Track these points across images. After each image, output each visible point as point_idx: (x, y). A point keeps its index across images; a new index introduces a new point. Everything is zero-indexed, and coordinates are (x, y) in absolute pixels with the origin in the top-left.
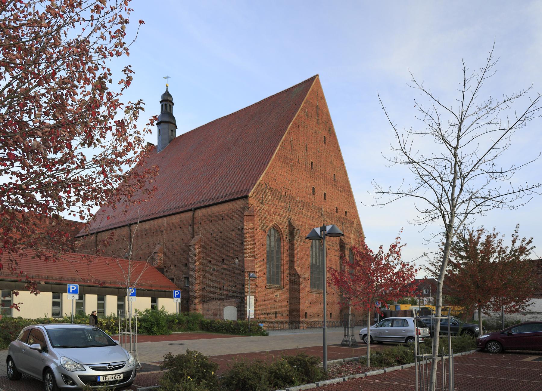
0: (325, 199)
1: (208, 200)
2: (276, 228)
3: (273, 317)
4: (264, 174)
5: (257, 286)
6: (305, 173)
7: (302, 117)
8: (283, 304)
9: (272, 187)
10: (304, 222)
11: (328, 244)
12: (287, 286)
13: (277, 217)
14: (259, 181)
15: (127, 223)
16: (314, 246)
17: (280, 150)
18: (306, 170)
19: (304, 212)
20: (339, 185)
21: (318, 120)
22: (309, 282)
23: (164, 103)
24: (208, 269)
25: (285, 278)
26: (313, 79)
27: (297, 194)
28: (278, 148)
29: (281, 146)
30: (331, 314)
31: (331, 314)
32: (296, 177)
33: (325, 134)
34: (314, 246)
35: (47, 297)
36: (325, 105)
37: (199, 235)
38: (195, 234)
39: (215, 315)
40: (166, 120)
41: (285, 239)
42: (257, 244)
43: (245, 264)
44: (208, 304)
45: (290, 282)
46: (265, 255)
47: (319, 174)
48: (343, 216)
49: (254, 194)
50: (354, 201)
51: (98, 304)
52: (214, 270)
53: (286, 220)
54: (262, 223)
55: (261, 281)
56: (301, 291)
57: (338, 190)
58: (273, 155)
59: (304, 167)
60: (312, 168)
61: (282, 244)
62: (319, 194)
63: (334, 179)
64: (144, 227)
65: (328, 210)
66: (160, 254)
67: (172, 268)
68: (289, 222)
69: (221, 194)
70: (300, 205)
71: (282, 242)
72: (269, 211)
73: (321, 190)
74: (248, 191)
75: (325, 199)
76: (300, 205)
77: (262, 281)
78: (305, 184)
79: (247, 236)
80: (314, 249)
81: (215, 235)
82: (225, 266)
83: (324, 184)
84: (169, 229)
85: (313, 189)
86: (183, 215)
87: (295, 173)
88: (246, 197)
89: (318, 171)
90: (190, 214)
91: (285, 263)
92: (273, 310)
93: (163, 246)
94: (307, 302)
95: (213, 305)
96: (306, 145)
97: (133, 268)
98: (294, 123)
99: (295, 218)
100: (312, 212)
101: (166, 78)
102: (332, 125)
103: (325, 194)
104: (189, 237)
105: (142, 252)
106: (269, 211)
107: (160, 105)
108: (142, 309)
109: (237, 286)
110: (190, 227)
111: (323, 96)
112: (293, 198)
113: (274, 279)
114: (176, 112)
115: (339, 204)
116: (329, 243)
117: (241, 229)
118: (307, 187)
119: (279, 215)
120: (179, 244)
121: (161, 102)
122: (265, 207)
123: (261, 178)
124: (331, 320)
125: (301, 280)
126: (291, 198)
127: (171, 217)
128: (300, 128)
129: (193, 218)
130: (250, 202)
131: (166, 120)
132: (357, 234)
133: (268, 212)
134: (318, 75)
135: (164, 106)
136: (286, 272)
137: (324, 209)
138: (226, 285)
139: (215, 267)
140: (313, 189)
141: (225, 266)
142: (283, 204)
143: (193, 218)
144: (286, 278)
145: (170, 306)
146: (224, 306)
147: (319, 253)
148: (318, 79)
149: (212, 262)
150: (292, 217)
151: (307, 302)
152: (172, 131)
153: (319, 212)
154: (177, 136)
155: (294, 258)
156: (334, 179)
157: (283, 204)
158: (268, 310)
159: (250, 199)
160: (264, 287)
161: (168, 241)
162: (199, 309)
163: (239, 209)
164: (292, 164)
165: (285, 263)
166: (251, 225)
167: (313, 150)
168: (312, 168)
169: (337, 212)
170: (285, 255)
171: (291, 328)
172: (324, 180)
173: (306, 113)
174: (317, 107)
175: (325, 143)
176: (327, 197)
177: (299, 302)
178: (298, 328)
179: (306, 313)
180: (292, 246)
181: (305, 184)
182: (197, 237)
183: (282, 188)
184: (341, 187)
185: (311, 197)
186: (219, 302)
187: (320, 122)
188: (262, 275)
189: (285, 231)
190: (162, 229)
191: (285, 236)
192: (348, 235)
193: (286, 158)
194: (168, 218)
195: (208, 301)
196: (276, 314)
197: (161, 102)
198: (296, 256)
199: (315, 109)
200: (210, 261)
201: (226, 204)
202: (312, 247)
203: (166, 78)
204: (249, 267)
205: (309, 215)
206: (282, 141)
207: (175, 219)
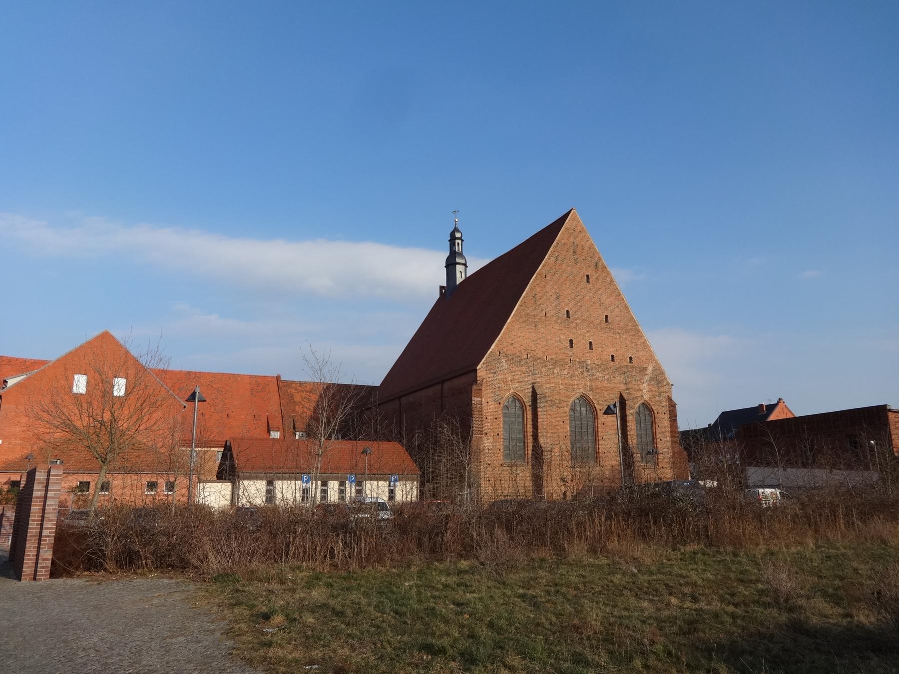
2: (516, 398)
6: (556, 326)
9: (509, 352)
13: (516, 384)
18: (559, 321)
19: (556, 371)
27: (544, 353)
42: (489, 418)
47: (579, 322)
62: (581, 345)
68: (533, 387)
89: (577, 319)
90: (439, 387)
97: (457, 435)
99: (544, 380)
100: (570, 369)
101: (455, 212)
106: (505, 381)
108: (507, 490)
112: (539, 358)
121: (278, 378)
126: (535, 359)
128: (548, 278)
132: (654, 383)
136: (530, 445)
137: (589, 362)
140: (571, 341)
154: (458, 283)
157: (524, 369)
176: (594, 346)
184: (619, 328)
185: (569, 352)
192: (636, 387)
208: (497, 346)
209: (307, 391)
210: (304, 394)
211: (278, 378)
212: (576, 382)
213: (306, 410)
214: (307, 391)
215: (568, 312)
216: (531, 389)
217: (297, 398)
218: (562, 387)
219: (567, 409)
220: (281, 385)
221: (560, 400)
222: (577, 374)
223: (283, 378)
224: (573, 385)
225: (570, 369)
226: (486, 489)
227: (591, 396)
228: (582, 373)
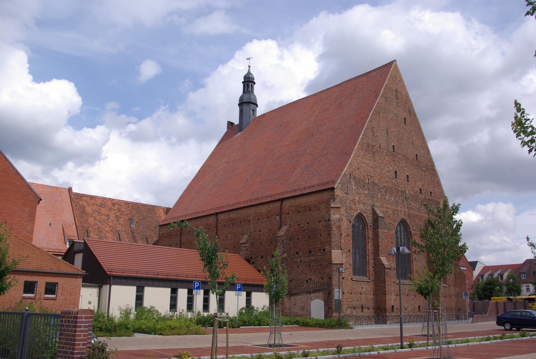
0: (408, 181)
1: (296, 190)
2: (360, 217)
3: (360, 310)
4: (348, 165)
5: (343, 278)
6: (387, 158)
7: (381, 103)
8: (370, 297)
9: (356, 176)
10: (388, 208)
11: (413, 230)
12: (372, 278)
14: (344, 172)
15: (213, 212)
16: (399, 232)
17: (362, 138)
18: (388, 154)
19: (387, 197)
20: (422, 165)
21: (397, 103)
22: (395, 272)
23: (247, 83)
24: (296, 260)
25: (371, 268)
26: (391, 63)
27: (379, 179)
28: (361, 137)
29: (363, 135)
30: (419, 307)
31: (419, 307)
32: (379, 162)
33: (406, 115)
34: (399, 232)
35: (167, 292)
36: (404, 87)
37: (286, 225)
38: (283, 224)
39: (303, 309)
40: (247, 102)
41: (369, 228)
42: (343, 235)
43: (333, 256)
44: (295, 297)
45: (375, 273)
46: (351, 246)
47: (400, 156)
48: (428, 197)
49: (340, 185)
50: (439, 179)
51: (204, 298)
52: (301, 261)
53: (369, 208)
54: (347, 213)
55: (347, 273)
56: (386, 283)
57: (421, 170)
58: (356, 145)
59: (386, 151)
60: (394, 151)
61: (367, 233)
62: (402, 177)
63: (417, 160)
64: (231, 216)
65: (412, 193)
66: (247, 245)
67: (259, 259)
69: (308, 185)
70: (383, 190)
71: (367, 230)
72: (353, 201)
73: (403, 172)
74: (334, 182)
75: (408, 181)
76: (383, 190)
77: (347, 272)
78: (388, 169)
79: (334, 228)
80: (399, 235)
81: (302, 226)
82: (312, 258)
83: (406, 166)
84: (257, 219)
85: (396, 172)
86: (271, 205)
87: (378, 159)
88: (333, 189)
90: (278, 204)
91: (370, 252)
92: (359, 304)
93: (249, 236)
94: (393, 294)
95: (299, 299)
96: (387, 130)
98: (375, 110)
100: (396, 197)
101: (248, 59)
102: (411, 105)
103: (408, 176)
104: (277, 228)
105: (228, 242)
106: (353, 201)
107: (242, 85)
109: (325, 279)
110: (278, 217)
111: (401, 79)
112: (376, 184)
113: (359, 269)
114: (257, 90)
115: (423, 185)
116: (414, 228)
117: (327, 220)
118: (389, 172)
119: (363, 204)
120: (266, 234)
121: (243, 83)
122: (350, 196)
123: (345, 169)
124: (419, 314)
125: (386, 270)
127: (259, 207)
128: (381, 114)
129: (281, 208)
130: (336, 193)
131: (247, 102)
133: (353, 201)
134: (395, 61)
135: (246, 86)
136: (371, 262)
138: (313, 278)
139: (302, 259)
140: (396, 172)
141: (312, 258)
142: (366, 192)
143: (281, 208)
144: (371, 268)
145: (261, 300)
146: (311, 299)
147: (404, 239)
148: (396, 64)
149: (299, 254)
150: (376, 204)
151: (393, 294)
152: (253, 110)
153: (402, 195)
155: (379, 247)
156: (417, 160)
157: (366, 192)
158: (354, 304)
159: (336, 190)
160: (350, 279)
161: (255, 231)
162: (286, 303)
163: (326, 200)
164: (374, 150)
165: (370, 252)
166: (338, 216)
167: (394, 133)
168: (394, 151)
169: (421, 193)
170: (370, 244)
171: (377, 322)
172: (406, 162)
173: (386, 98)
174: (396, 90)
175: (405, 124)
176: (410, 179)
177: (385, 294)
178: (386, 323)
179: (393, 306)
180: (376, 235)
181: (388, 169)
182: (285, 228)
183: (366, 176)
186: (306, 296)
187: (399, 104)
188: (349, 266)
189: (369, 220)
190: (249, 219)
191: (369, 225)
193: (368, 145)
194: (256, 208)
195: (295, 294)
196: (362, 307)
197: (243, 83)
198: (380, 244)
199: (394, 93)
200: (297, 253)
201: (314, 195)
202: (396, 233)
203: (248, 59)
204: (336, 259)
205: (393, 200)
206: (364, 130)
207: (263, 209)
208: (348, 169)
209: (97, 205)
210: (95, 207)
211: (70, 190)
212: (399, 209)
213: (97, 222)
214: (97, 205)
215: (393, 146)
216: (371, 211)
217: (89, 210)
218: (391, 212)
219: (394, 232)
220: (73, 196)
221: (390, 223)
222: (400, 201)
223: (75, 190)
224: (397, 211)
225: (396, 197)
226: (80, 308)
227: (408, 222)
228: (403, 201)
